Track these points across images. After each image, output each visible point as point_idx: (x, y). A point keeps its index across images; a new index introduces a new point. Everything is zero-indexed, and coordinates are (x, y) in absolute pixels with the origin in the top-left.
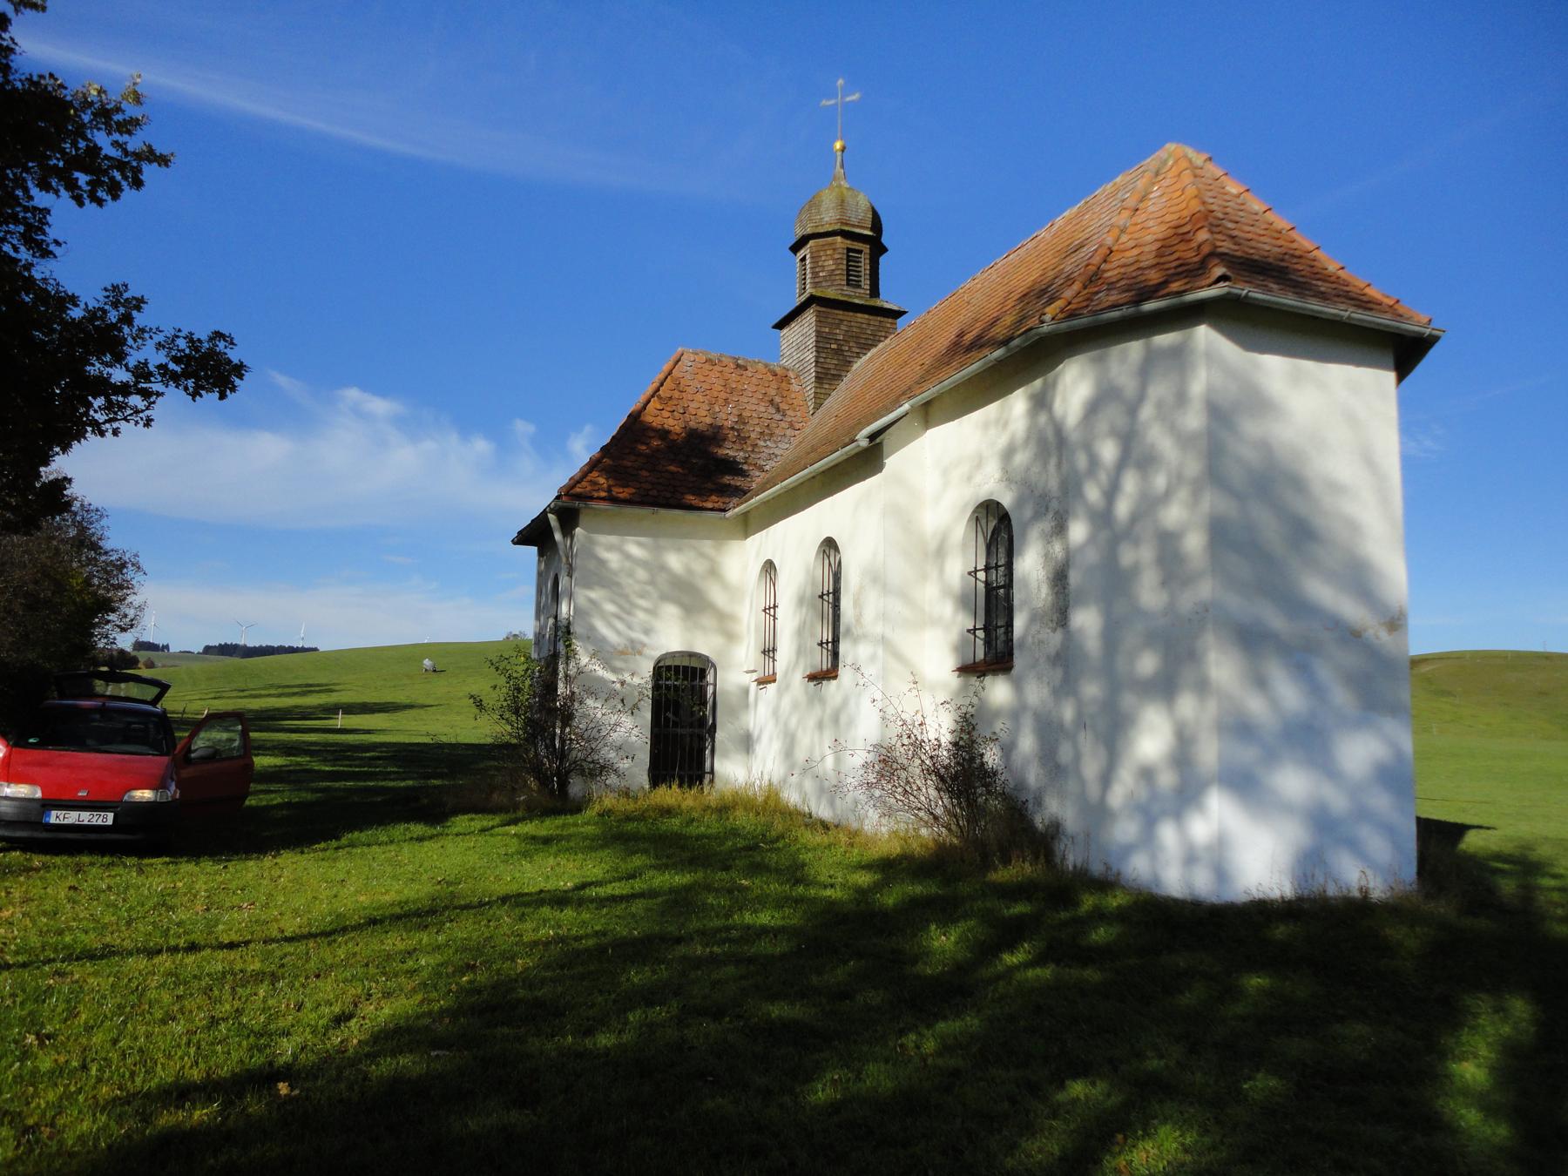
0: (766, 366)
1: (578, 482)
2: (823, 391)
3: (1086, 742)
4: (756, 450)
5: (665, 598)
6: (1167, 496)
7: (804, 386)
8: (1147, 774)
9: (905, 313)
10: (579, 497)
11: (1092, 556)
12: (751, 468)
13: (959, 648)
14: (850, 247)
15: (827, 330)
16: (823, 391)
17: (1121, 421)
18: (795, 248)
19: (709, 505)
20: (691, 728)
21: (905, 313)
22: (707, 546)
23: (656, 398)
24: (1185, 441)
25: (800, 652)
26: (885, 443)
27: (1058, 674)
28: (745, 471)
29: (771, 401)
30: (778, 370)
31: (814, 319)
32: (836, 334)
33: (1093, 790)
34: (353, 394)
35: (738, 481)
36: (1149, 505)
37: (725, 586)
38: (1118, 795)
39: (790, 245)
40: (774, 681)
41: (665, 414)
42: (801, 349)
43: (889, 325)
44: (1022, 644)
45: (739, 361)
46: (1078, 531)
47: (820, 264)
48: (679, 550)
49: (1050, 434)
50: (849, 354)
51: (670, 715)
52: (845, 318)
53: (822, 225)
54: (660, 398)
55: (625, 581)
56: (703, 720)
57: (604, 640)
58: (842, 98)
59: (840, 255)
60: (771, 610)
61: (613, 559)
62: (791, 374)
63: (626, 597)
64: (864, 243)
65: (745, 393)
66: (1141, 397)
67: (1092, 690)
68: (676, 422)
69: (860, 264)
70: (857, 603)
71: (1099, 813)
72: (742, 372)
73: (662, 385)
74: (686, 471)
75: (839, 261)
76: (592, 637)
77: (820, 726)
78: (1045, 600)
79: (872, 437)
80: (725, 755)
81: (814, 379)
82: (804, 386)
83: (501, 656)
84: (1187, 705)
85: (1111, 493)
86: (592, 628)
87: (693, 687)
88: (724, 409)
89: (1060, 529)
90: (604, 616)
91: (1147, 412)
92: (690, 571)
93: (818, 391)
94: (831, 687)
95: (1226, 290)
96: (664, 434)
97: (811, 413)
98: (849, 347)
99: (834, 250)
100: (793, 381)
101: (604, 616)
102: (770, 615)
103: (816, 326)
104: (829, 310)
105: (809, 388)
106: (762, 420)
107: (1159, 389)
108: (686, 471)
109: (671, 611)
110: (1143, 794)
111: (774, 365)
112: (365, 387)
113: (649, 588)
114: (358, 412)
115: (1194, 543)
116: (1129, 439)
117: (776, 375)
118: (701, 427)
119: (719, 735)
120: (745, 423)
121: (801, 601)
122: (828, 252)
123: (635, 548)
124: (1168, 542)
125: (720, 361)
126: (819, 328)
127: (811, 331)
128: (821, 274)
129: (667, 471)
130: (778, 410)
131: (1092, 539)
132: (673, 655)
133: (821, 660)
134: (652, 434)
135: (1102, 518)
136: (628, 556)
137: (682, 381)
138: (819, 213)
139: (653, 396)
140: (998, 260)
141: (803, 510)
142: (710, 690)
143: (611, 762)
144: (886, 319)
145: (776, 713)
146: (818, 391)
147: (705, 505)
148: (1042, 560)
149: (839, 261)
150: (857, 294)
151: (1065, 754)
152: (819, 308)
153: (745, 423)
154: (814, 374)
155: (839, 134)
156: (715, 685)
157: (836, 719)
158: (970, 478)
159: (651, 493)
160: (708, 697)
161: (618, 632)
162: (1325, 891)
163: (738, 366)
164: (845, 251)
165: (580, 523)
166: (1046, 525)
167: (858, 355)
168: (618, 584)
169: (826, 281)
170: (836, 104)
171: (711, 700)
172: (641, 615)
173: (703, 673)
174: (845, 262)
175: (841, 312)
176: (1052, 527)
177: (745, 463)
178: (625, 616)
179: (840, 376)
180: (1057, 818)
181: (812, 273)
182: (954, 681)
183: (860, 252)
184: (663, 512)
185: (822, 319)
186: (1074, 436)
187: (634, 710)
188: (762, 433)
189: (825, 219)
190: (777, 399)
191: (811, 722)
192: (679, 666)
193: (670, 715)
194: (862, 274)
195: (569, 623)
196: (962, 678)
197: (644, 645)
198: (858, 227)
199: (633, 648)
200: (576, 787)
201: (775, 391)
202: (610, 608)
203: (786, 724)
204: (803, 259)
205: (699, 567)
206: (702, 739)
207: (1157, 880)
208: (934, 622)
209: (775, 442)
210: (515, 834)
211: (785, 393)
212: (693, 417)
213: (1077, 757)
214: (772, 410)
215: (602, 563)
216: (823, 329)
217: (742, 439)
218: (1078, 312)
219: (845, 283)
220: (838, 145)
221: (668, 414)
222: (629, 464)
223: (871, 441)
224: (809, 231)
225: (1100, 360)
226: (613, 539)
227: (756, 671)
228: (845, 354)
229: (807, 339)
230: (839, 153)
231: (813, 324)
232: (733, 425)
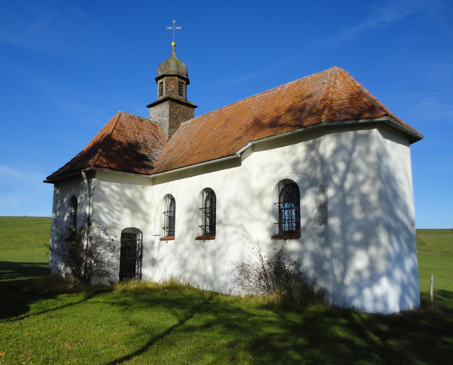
3: (335, 262)
5: (125, 206)
6: (363, 182)
7: (162, 130)
8: (359, 273)
9: (197, 107)
10: (98, 166)
11: (336, 200)
17: (346, 157)
18: (157, 79)
19: (143, 172)
20: (134, 257)
21: (197, 107)
22: (139, 187)
23: (115, 129)
24: (369, 165)
27: (323, 240)
29: (153, 134)
30: (153, 122)
31: (169, 106)
33: (339, 279)
35: (148, 163)
36: (356, 185)
37: (146, 203)
38: (348, 280)
39: (156, 77)
42: (161, 116)
43: (192, 111)
44: (305, 229)
46: (330, 192)
47: (169, 86)
48: (130, 188)
49: (317, 159)
50: (179, 119)
51: (127, 252)
53: (170, 72)
55: (111, 199)
58: (175, 27)
59: (177, 84)
62: (157, 125)
63: (111, 205)
64: (184, 80)
66: (353, 150)
67: (337, 245)
70: (225, 212)
71: (341, 286)
73: (116, 125)
75: (176, 86)
76: (100, 222)
78: (316, 214)
80: (145, 267)
81: (168, 128)
82: (162, 130)
84: (373, 250)
85: (343, 179)
86: (99, 218)
89: (323, 190)
90: (103, 213)
91: (355, 155)
92: (134, 197)
93: (170, 132)
94: (210, 243)
95: (388, 119)
96: (120, 143)
99: (174, 81)
101: (103, 213)
105: (165, 131)
106: (151, 141)
107: (360, 148)
109: (127, 211)
110: (357, 279)
113: (120, 203)
115: (373, 198)
116: (349, 163)
118: (132, 142)
122: (172, 82)
123: (115, 187)
124: (364, 198)
129: (125, 158)
131: (336, 195)
132: (128, 229)
134: (117, 143)
135: (340, 188)
136: (112, 190)
138: (169, 67)
139: (114, 129)
140: (256, 95)
141: (191, 177)
146: (170, 132)
147: (140, 172)
148: (314, 201)
149: (176, 86)
150: (182, 99)
151: (326, 266)
152: (170, 102)
154: (168, 126)
155: (173, 40)
157: (213, 254)
158: (276, 171)
161: (109, 220)
162: (409, 309)
163: (140, 120)
164: (178, 82)
165: (96, 176)
166: (316, 189)
168: (108, 201)
170: (172, 29)
172: (117, 213)
175: (177, 104)
176: (319, 190)
177: (149, 157)
178: (111, 213)
180: (324, 288)
182: (269, 241)
183: (183, 83)
184: (128, 174)
186: (329, 161)
187: (113, 251)
188: (152, 146)
189: (172, 70)
190: (155, 134)
193: (127, 252)
194: (183, 91)
196: (273, 240)
197: (118, 225)
198: (182, 74)
199: (114, 226)
202: (106, 210)
205: (137, 195)
207: (363, 308)
208: (260, 220)
209: (157, 150)
210: (102, 302)
212: (129, 138)
213: (332, 267)
215: (103, 192)
217: (146, 148)
218: (333, 120)
219: (178, 94)
220: (173, 44)
221: (120, 136)
222: (112, 155)
224: (165, 73)
225: (338, 136)
226: (107, 183)
227: (160, 235)
228: (179, 119)
230: (173, 47)
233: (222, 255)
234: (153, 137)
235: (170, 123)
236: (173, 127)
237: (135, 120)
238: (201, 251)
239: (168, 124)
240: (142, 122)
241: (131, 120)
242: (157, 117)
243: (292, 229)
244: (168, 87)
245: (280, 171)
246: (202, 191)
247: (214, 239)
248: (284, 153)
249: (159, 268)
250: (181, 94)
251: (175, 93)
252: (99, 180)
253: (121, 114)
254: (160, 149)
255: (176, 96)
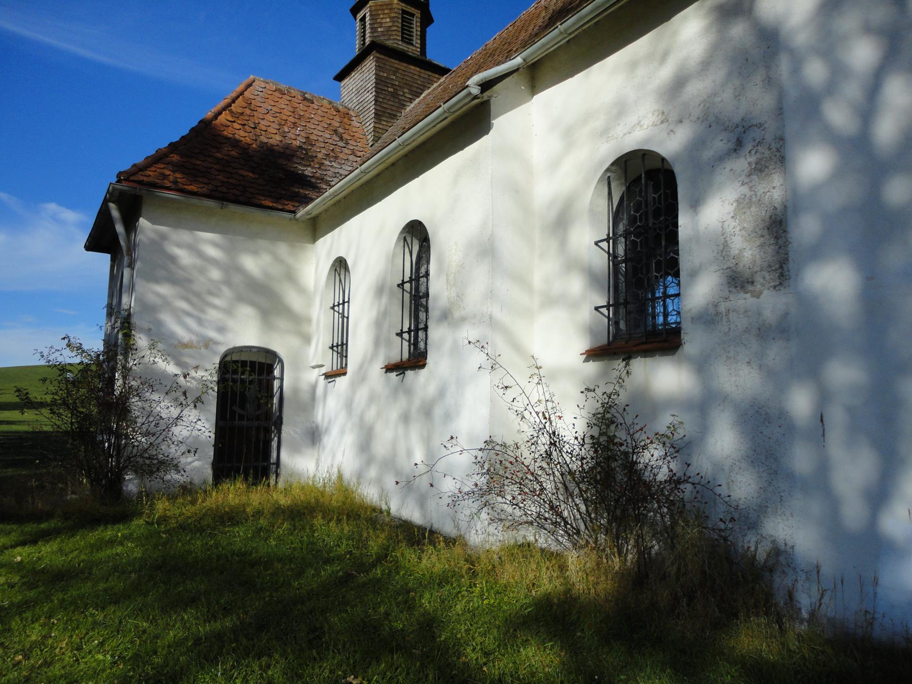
0: (330, 103)
1: (141, 170)
2: (381, 126)
4: (323, 168)
5: (240, 298)
7: (363, 123)
12: (318, 182)
13: (592, 331)
14: (404, 8)
15: (385, 75)
16: (381, 126)
22: (282, 249)
25: (377, 342)
26: (493, 101)
28: (313, 183)
29: (335, 131)
30: (340, 108)
31: (374, 64)
32: (392, 79)
34: (52, 207)
40: (345, 374)
41: (236, 126)
42: (360, 93)
45: (306, 95)
47: (378, 21)
48: (255, 253)
50: (403, 98)
52: (401, 68)
54: (231, 111)
56: (268, 414)
57: (172, 335)
60: (340, 307)
61: (185, 257)
62: (351, 113)
65: (312, 121)
68: (247, 134)
69: (412, 30)
72: (309, 104)
74: (257, 176)
75: (395, 19)
77: (405, 418)
79: (486, 86)
82: (363, 123)
83: (52, 347)
86: (159, 324)
87: (260, 381)
88: (293, 131)
93: (377, 125)
94: (418, 379)
96: (235, 143)
97: (370, 145)
98: (404, 92)
99: (391, 9)
100: (354, 118)
102: (339, 312)
103: (376, 69)
104: (386, 58)
105: (368, 124)
106: (327, 144)
108: (257, 176)
109: (246, 312)
111: (338, 104)
112: (61, 203)
114: (55, 219)
117: (339, 112)
119: (285, 429)
120: (312, 145)
121: (380, 290)
122: (386, 11)
125: (288, 92)
126: (378, 72)
127: (371, 75)
128: (379, 30)
130: (341, 139)
133: (399, 350)
136: (200, 255)
137: (253, 102)
141: (380, 200)
142: (276, 384)
143: (171, 456)
144: (434, 75)
145: (349, 405)
146: (377, 125)
152: (378, 55)
153: (312, 145)
154: (373, 111)
156: (282, 379)
157: (427, 411)
159: (219, 189)
160: (275, 391)
161: (188, 329)
163: (305, 99)
164: (401, 12)
165: (143, 215)
167: (411, 101)
168: (190, 281)
169: (384, 35)
171: (278, 394)
173: (270, 369)
174: (400, 21)
175: (397, 62)
179: (396, 116)
181: (371, 28)
183: (413, 15)
184: (233, 208)
185: (381, 65)
186: (802, 39)
188: (327, 155)
190: (341, 130)
191: (394, 414)
192: (255, 362)
195: (129, 315)
200: (131, 484)
201: (339, 124)
203: (361, 418)
204: (363, 19)
206: (268, 431)
211: (347, 127)
212: (263, 133)
214: (335, 138)
215: (173, 259)
216: (382, 74)
217: (309, 158)
221: (239, 127)
223: (483, 91)
228: (400, 98)
229: (367, 83)
231: (373, 68)
232: (301, 144)
233: (448, 417)
234: (334, 136)
235: (378, 104)
236: (387, 115)
237: (289, 98)
238: (401, 403)
239: (373, 107)
240: (311, 105)
241: (280, 96)
242: (354, 98)
243: (666, 322)
244: (377, 23)
245: (619, 130)
246: (402, 233)
247: (120, 173)
248: (633, 66)
249: (324, 448)
250: (407, 38)
251: (392, 38)
252: (153, 224)
253: (254, 81)
254: (349, 164)
255: (395, 42)
